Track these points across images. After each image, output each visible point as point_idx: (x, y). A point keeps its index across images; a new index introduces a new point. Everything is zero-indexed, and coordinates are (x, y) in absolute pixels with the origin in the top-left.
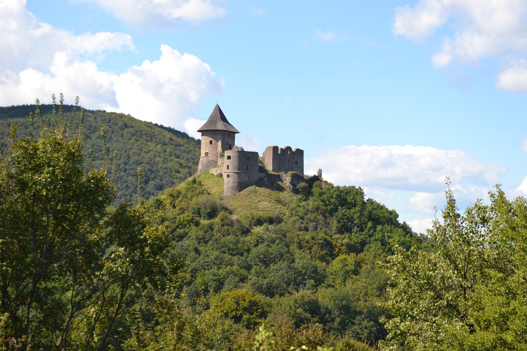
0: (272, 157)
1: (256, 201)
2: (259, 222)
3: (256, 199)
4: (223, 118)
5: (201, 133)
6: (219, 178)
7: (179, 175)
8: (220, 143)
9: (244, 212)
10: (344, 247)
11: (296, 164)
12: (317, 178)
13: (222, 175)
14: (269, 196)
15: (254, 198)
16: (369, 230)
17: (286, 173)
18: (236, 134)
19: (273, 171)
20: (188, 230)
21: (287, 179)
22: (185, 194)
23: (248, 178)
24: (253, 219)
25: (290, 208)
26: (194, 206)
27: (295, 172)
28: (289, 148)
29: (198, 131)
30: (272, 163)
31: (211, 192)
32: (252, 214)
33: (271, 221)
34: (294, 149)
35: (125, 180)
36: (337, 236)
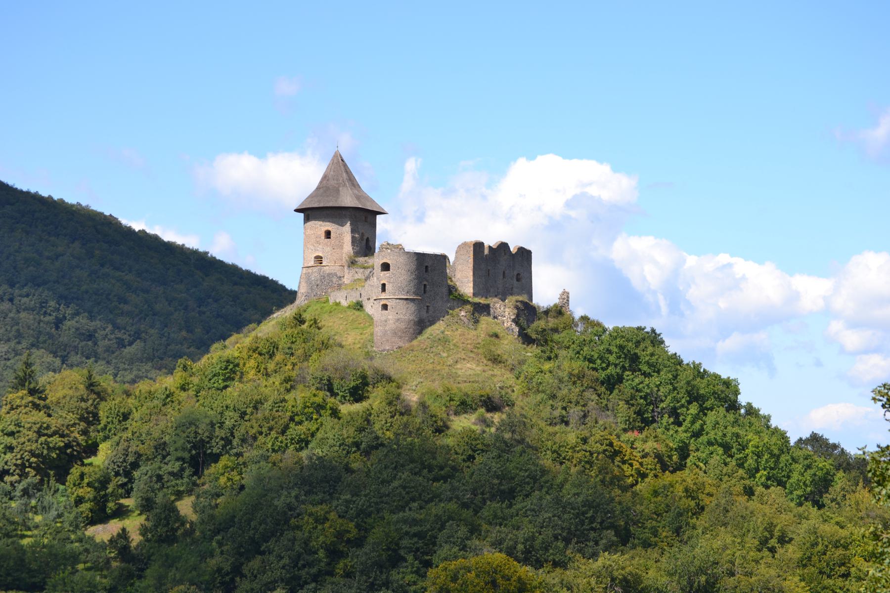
0: (471, 266)
1: (450, 361)
2: (464, 406)
3: (448, 357)
4: (352, 182)
5: (302, 215)
6: (357, 313)
7: (126, 308)
8: (347, 237)
9: (427, 384)
10: (648, 460)
11: (518, 280)
12: (559, 311)
13: (361, 306)
14: (475, 350)
15: (445, 355)
16: (693, 422)
17: (503, 300)
18: (378, 217)
19: (475, 295)
20: (316, 426)
21: (507, 314)
22: (289, 348)
23: (427, 312)
24: (451, 400)
25: (522, 376)
26: (319, 374)
27: (520, 298)
28: (504, 246)
29: (297, 211)
30: (471, 279)
31: (344, 343)
32: (449, 390)
33: (491, 405)
34: (513, 249)
35: (13, 319)
36: (631, 436)
